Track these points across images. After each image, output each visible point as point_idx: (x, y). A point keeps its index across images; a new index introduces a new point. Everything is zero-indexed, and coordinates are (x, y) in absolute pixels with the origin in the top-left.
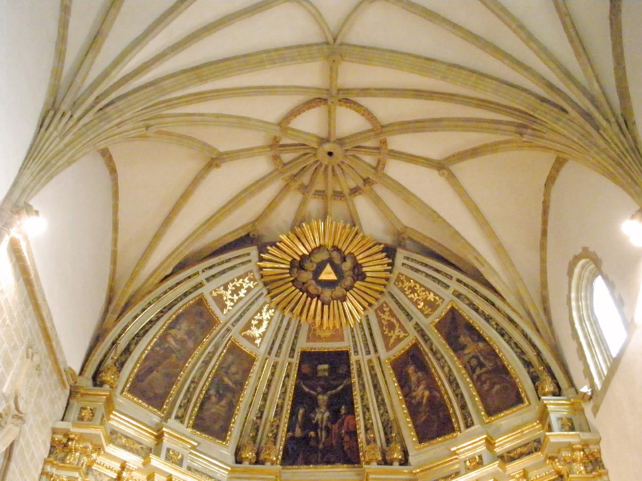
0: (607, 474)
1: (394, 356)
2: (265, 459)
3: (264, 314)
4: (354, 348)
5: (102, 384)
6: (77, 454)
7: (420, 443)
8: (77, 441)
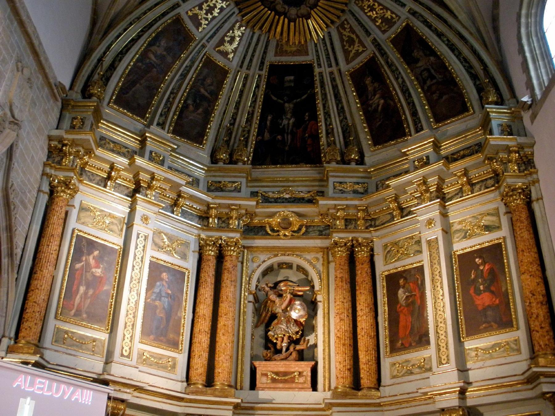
0: (537, 173)
1: (353, 68)
2: (237, 159)
3: (236, 31)
4: (318, 61)
5: (90, 96)
6: (71, 157)
7: (375, 145)
8: (70, 146)
